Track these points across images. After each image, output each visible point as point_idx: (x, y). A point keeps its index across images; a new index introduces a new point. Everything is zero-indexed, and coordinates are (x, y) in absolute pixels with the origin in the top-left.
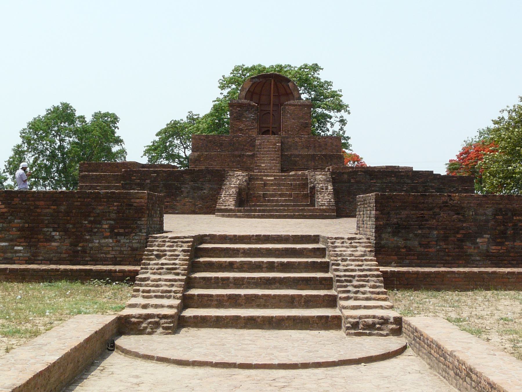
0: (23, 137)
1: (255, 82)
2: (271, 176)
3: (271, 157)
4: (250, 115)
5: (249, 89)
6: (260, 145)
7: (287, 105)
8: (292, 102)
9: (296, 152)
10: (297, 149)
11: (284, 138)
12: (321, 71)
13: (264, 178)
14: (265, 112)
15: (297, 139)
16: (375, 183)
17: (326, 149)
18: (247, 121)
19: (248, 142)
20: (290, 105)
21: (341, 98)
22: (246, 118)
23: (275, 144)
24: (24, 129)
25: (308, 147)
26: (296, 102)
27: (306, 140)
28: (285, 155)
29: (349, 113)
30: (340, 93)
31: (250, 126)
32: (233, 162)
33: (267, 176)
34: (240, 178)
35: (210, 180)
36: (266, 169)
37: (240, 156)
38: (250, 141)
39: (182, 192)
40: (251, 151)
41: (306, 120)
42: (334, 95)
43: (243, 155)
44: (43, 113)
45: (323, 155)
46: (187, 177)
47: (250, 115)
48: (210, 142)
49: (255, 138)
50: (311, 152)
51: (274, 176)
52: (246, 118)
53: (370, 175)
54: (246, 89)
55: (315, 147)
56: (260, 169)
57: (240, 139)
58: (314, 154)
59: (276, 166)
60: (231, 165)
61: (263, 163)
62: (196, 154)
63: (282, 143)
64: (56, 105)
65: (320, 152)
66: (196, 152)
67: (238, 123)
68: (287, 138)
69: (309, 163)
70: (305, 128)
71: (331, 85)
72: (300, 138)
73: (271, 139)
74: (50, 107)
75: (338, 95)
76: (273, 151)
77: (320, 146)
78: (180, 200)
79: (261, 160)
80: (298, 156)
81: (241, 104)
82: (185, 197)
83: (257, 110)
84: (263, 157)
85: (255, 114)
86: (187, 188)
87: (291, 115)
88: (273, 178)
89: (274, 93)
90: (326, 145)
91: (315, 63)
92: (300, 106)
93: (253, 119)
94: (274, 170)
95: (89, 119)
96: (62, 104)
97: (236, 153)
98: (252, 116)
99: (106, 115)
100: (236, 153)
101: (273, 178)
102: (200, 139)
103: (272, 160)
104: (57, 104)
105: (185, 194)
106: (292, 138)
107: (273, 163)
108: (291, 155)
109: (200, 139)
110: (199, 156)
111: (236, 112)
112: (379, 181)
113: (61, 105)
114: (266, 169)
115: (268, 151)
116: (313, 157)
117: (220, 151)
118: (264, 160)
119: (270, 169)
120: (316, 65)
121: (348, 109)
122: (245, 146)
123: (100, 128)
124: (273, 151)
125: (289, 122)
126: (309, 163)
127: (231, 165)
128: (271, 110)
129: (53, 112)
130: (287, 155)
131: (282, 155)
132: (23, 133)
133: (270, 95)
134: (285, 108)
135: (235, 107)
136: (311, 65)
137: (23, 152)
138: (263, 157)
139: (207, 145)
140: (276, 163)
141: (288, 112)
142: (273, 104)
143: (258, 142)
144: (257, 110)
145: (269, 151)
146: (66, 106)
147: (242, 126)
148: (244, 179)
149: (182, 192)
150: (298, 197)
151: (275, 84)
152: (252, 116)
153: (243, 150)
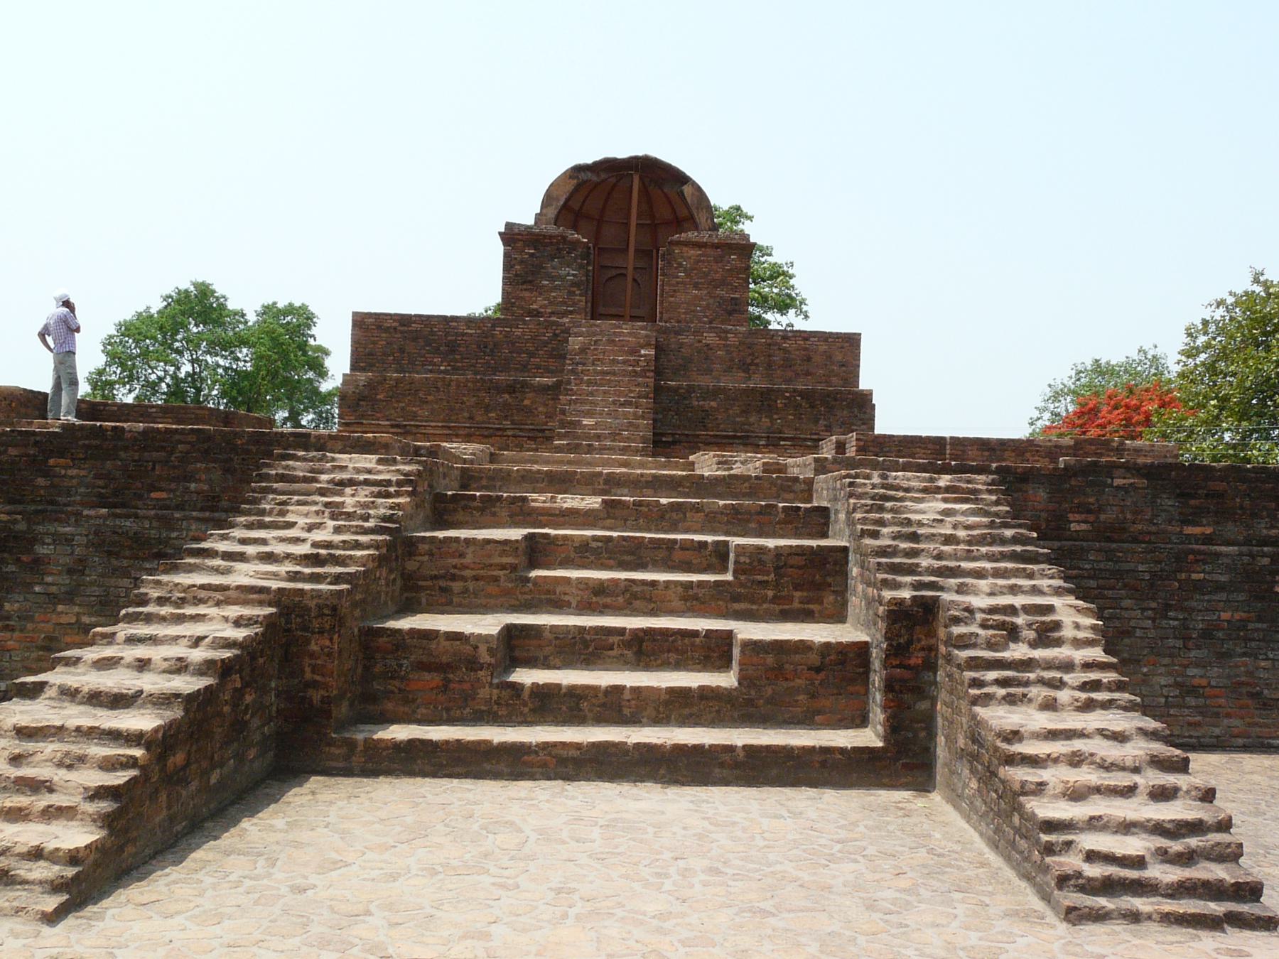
0: (108, 354)
1: (584, 182)
2: (588, 484)
3: (619, 394)
4: (563, 272)
5: (567, 200)
6: (583, 350)
7: (678, 243)
8: (692, 235)
9: (706, 381)
10: (709, 371)
11: (665, 331)
12: (747, 222)
13: (539, 500)
14: (614, 272)
15: (710, 338)
16: (1208, 540)
17: (808, 374)
18: (556, 288)
19: (546, 344)
20: (687, 243)
21: (792, 282)
22: (552, 278)
23: (634, 351)
24: (111, 337)
25: (746, 367)
26: (705, 236)
27: (741, 343)
28: (669, 389)
29: (806, 317)
30: (791, 272)
31: (564, 303)
32: (488, 409)
33: (562, 482)
34: (349, 500)
35: (216, 498)
36: (598, 437)
37: (511, 389)
38: (551, 339)
39: (38, 566)
40: (551, 372)
41: (735, 289)
42: (778, 274)
43: (525, 385)
44: (157, 305)
45: (803, 394)
46: (74, 474)
47: (563, 272)
48: (415, 340)
49: (567, 331)
50: (758, 382)
51: (612, 482)
52: (552, 278)
53: (1183, 496)
54: (558, 200)
55: (769, 366)
56: (576, 437)
57: (518, 332)
58: (770, 390)
59: (637, 427)
60: (479, 418)
61: (589, 414)
62: (362, 377)
63: (658, 348)
64: (182, 287)
65: (788, 381)
66: (363, 369)
67: (527, 294)
68: (677, 333)
69: (752, 420)
70: (730, 313)
71: (770, 255)
72: (723, 334)
73: (620, 334)
74: (169, 290)
75: (785, 274)
76: (625, 373)
77: (788, 364)
78: (25, 617)
79: (583, 402)
80: (715, 393)
81: (538, 235)
82: (53, 599)
83: (586, 256)
84: (591, 394)
85: (581, 267)
86: (68, 540)
87: (688, 276)
88: (594, 502)
89: (639, 217)
90: (809, 359)
91: (734, 204)
92: (716, 246)
93: (574, 284)
94: (628, 439)
95: (252, 318)
96: (196, 285)
97: (501, 377)
98: (570, 273)
99: (290, 310)
100: (501, 377)
101: (594, 502)
102: (379, 327)
103: (622, 405)
104: (185, 285)
105: (55, 580)
106: (696, 333)
107: (625, 415)
108: (691, 389)
109: (379, 327)
110: (370, 385)
111: (522, 262)
112: (1231, 530)
113: (192, 288)
114: (598, 437)
115: (607, 373)
116: (764, 401)
117: (445, 372)
118: (595, 404)
119: (615, 436)
120: (738, 208)
121: (804, 308)
122: (532, 355)
123: (273, 339)
124: (625, 373)
125: (682, 297)
126: (752, 420)
127: (479, 418)
128: (631, 268)
129: (178, 302)
130: (676, 390)
131: (658, 390)
132: (110, 344)
133: (627, 225)
134: (670, 253)
135: (520, 244)
136: (726, 208)
137: (111, 384)
138: (591, 394)
139: (402, 350)
140: (636, 417)
141: (680, 265)
142: (636, 251)
143: (575, 343)
144: (586, 256)
145: (614, 374)
146: (204, 291)
147: (538, 303)
148: (382, 507)
149: (38, 566)
150: (778, 672)
151: (644, 191)
152: (570, 273)
153: (524, 368)
